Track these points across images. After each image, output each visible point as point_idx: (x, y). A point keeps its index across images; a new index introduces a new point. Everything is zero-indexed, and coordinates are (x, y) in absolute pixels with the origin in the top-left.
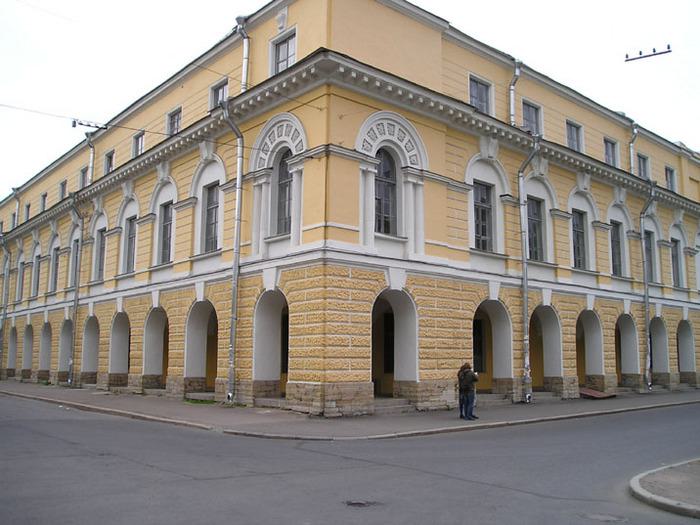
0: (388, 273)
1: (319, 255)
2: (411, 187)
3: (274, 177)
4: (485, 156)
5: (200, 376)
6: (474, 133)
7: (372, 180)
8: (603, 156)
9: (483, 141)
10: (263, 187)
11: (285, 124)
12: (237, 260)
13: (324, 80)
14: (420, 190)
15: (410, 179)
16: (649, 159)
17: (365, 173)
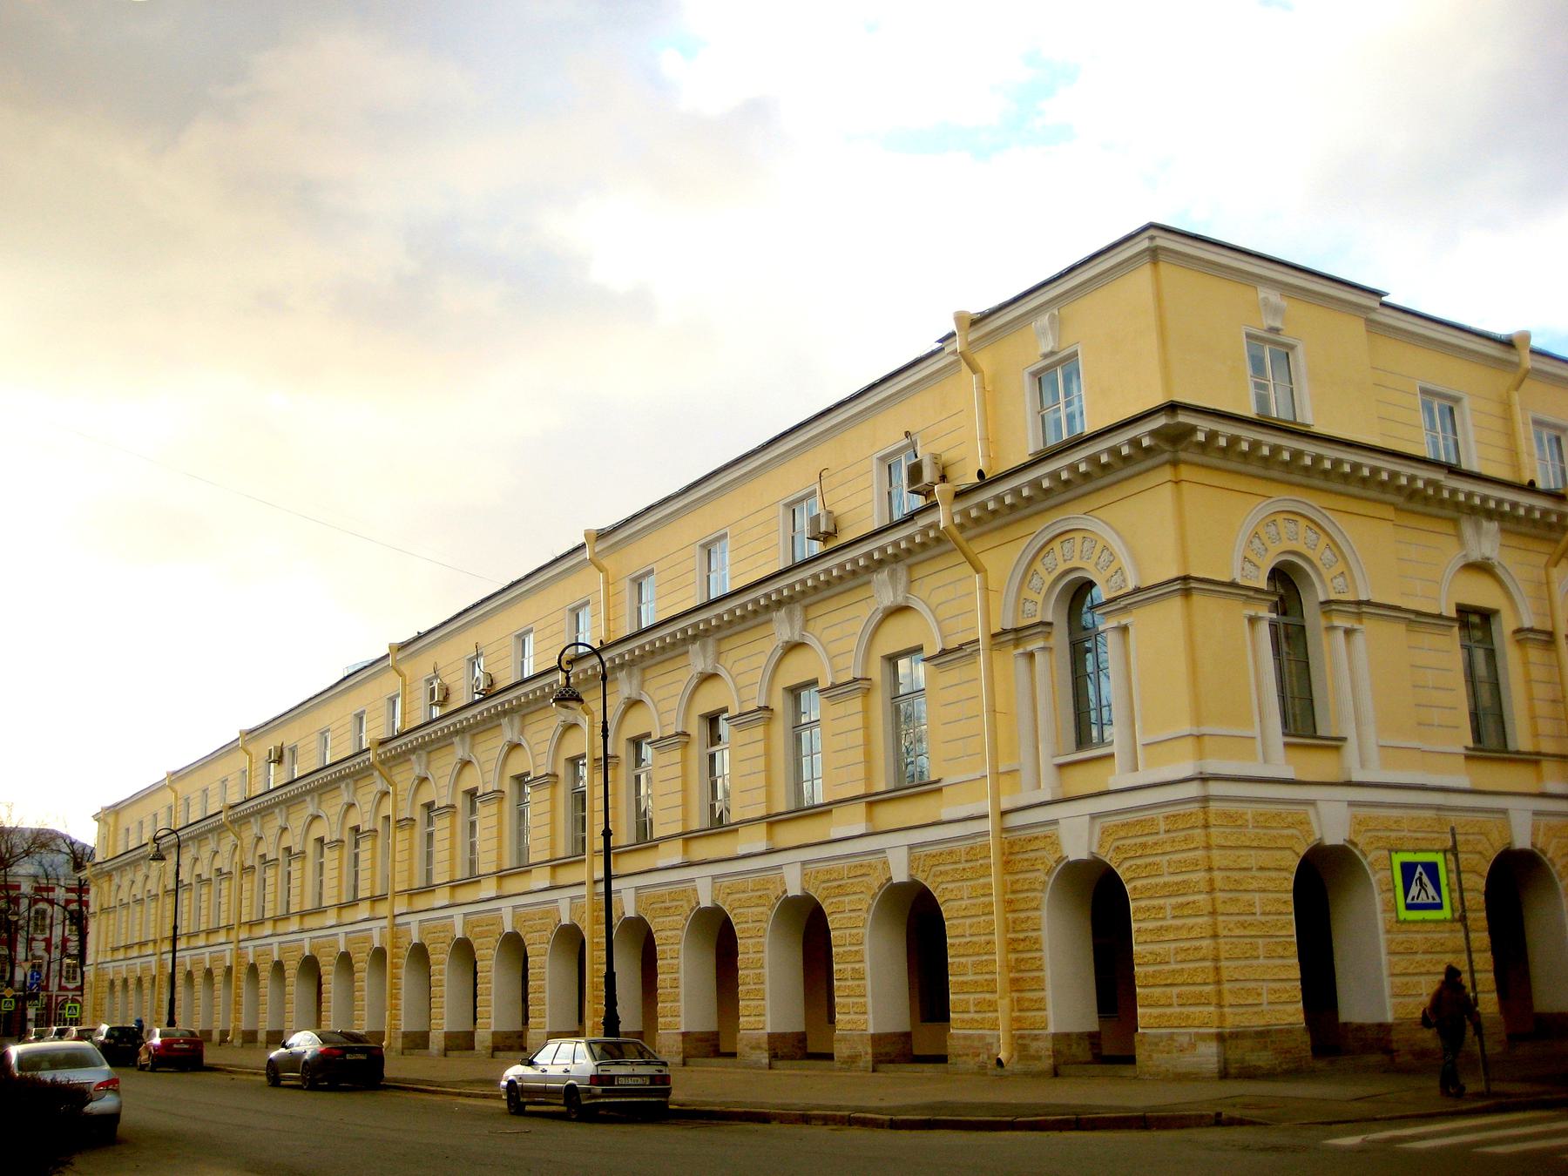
0: (1317, 813)
1: (1193, 790)
2: (1340, 635)
3: (1060, 638)
4: (1475, 556)
5: (636, 1030)
6: (1448, 513)
7: (1264, 630)
8: (1425, 437)
9: (1467, 528)
10: (1039, 657)
11: (1078, 536)
12: (996, 799)
13: (1166, 456)
14: (1358, 639)
15: (1336, 623)
16: (1300, 349)
17: (1253, 621)
